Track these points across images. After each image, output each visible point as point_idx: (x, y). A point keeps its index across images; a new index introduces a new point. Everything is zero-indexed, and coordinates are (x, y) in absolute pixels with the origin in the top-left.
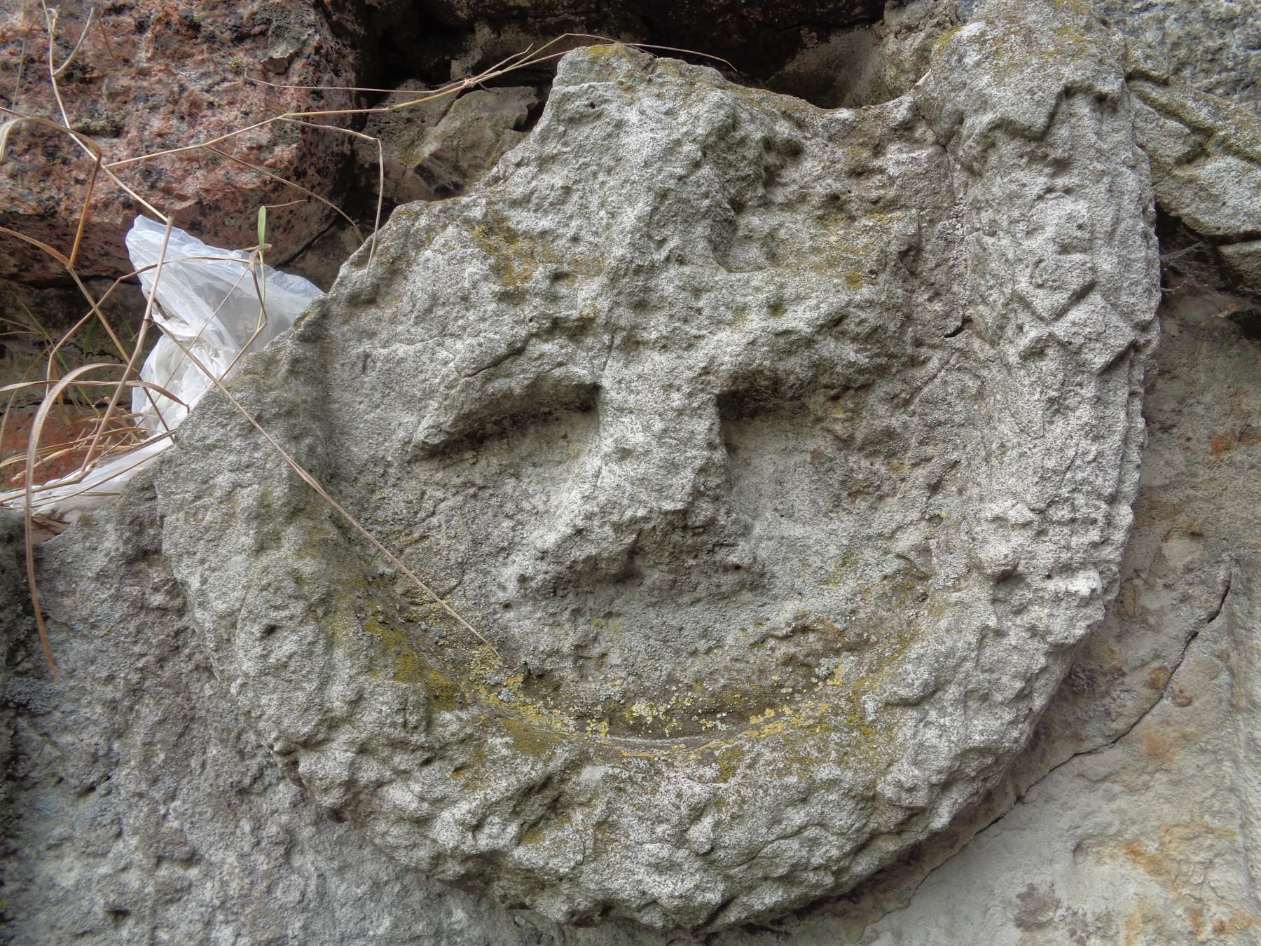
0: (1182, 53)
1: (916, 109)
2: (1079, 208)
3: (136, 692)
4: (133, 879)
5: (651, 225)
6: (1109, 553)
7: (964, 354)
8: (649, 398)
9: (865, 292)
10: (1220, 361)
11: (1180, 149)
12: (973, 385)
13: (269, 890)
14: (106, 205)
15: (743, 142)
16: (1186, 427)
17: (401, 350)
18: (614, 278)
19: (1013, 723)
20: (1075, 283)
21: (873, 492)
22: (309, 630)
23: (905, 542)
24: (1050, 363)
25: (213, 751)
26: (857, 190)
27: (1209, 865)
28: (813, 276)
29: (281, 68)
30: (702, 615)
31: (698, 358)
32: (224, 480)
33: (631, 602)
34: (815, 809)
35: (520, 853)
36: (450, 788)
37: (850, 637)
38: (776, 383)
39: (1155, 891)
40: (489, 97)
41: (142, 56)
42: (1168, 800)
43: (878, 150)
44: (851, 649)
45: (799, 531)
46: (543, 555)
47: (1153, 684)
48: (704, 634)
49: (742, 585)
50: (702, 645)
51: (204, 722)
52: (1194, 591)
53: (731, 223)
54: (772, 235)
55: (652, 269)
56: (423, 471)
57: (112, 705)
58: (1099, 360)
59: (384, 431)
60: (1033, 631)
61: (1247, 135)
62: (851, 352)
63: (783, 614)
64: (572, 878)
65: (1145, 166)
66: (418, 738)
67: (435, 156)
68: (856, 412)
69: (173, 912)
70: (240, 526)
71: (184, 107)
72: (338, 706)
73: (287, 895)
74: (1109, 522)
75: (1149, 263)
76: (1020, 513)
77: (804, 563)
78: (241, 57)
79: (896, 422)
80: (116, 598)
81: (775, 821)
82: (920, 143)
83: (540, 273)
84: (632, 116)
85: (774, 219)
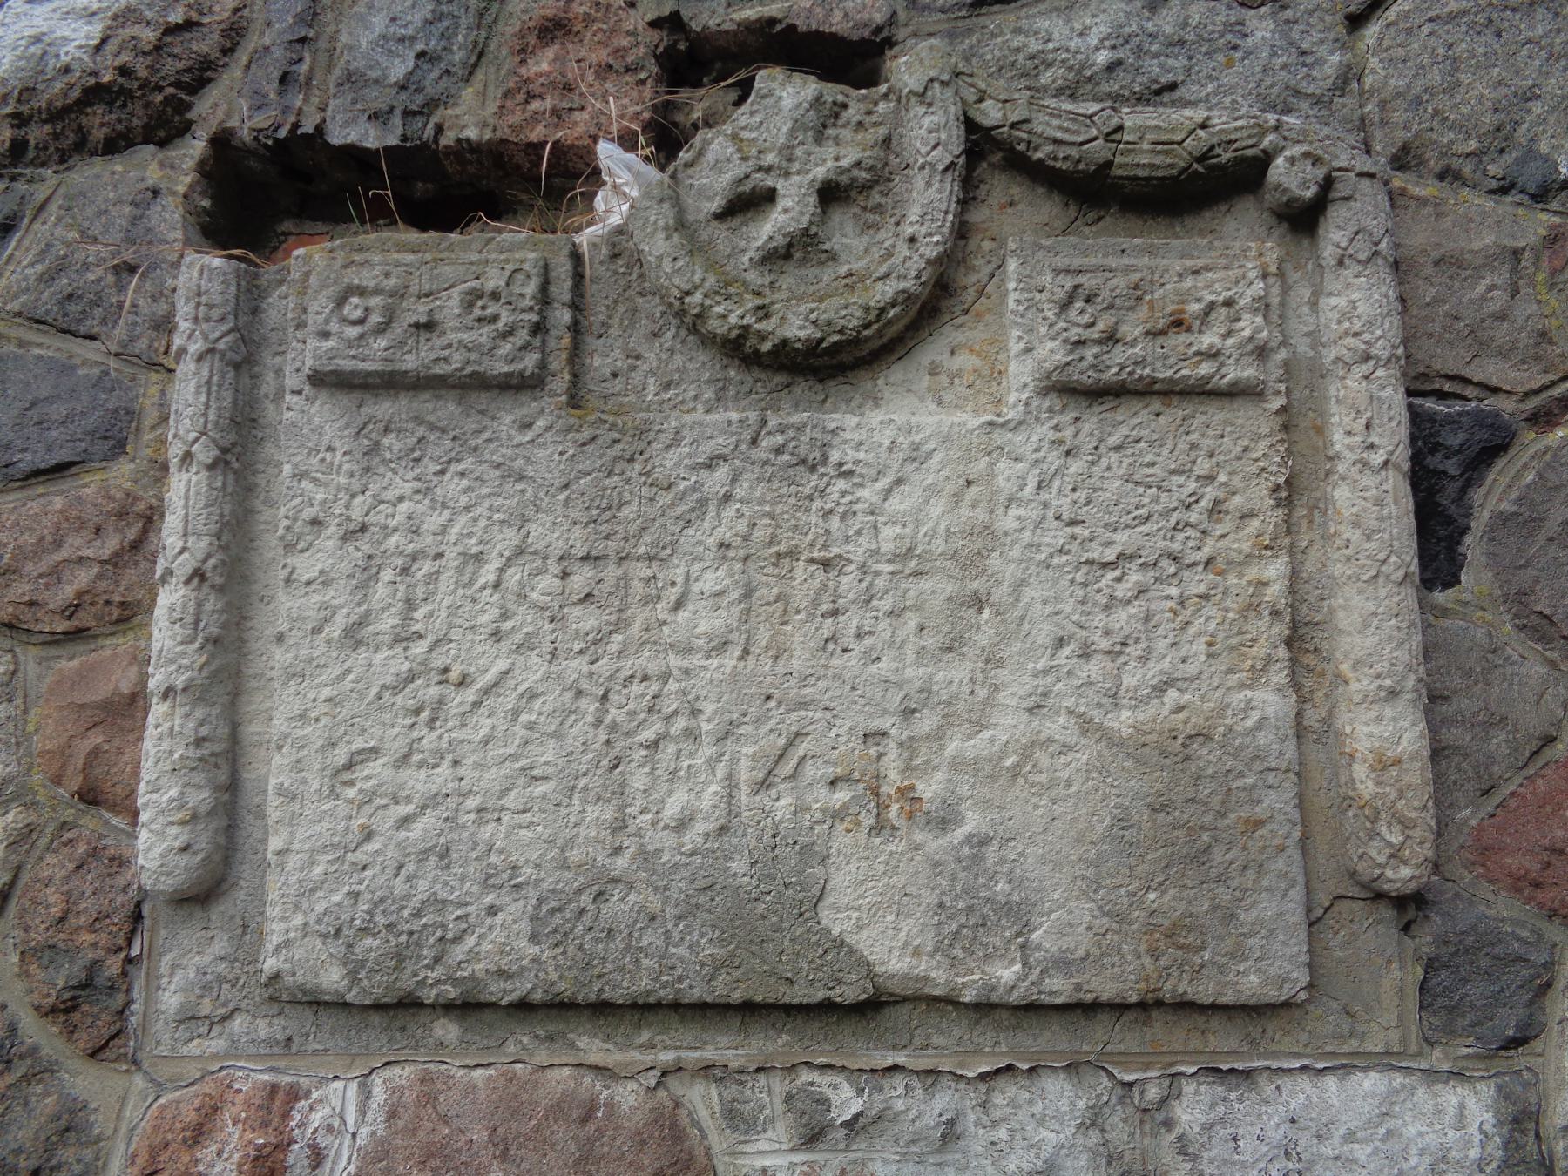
2: (935, 118)
3: (616, 302)
4: (619, 363)
5: (792, 131)
8: (793, 191)
9: (868, 153)
11: (975, 98)
16: (990, 200)
20: (933, 143)
23: (887, 244)
24: (927, 171)
26: (868, 119)
29: (643, 82)
30: (816, 271)
31: (810, 176)
32: (653, 218)
33: (789, 267)
35: (758, 326)
36: (734, 307)
38: (837, 184)
40: (36, 226)
43: (876, 104)
55: (793, 147)
56: (715, 224)
58: (940, 167)
59: (699, 210)
60: (921, 256)
62: (864, 174)
63: (843, 270)
64: (772, 333)
68: (868, 197)
73: (672, 367)
78: (628, 78)
79: (883, 201)
84: (784, 94)
85: (837, 131)
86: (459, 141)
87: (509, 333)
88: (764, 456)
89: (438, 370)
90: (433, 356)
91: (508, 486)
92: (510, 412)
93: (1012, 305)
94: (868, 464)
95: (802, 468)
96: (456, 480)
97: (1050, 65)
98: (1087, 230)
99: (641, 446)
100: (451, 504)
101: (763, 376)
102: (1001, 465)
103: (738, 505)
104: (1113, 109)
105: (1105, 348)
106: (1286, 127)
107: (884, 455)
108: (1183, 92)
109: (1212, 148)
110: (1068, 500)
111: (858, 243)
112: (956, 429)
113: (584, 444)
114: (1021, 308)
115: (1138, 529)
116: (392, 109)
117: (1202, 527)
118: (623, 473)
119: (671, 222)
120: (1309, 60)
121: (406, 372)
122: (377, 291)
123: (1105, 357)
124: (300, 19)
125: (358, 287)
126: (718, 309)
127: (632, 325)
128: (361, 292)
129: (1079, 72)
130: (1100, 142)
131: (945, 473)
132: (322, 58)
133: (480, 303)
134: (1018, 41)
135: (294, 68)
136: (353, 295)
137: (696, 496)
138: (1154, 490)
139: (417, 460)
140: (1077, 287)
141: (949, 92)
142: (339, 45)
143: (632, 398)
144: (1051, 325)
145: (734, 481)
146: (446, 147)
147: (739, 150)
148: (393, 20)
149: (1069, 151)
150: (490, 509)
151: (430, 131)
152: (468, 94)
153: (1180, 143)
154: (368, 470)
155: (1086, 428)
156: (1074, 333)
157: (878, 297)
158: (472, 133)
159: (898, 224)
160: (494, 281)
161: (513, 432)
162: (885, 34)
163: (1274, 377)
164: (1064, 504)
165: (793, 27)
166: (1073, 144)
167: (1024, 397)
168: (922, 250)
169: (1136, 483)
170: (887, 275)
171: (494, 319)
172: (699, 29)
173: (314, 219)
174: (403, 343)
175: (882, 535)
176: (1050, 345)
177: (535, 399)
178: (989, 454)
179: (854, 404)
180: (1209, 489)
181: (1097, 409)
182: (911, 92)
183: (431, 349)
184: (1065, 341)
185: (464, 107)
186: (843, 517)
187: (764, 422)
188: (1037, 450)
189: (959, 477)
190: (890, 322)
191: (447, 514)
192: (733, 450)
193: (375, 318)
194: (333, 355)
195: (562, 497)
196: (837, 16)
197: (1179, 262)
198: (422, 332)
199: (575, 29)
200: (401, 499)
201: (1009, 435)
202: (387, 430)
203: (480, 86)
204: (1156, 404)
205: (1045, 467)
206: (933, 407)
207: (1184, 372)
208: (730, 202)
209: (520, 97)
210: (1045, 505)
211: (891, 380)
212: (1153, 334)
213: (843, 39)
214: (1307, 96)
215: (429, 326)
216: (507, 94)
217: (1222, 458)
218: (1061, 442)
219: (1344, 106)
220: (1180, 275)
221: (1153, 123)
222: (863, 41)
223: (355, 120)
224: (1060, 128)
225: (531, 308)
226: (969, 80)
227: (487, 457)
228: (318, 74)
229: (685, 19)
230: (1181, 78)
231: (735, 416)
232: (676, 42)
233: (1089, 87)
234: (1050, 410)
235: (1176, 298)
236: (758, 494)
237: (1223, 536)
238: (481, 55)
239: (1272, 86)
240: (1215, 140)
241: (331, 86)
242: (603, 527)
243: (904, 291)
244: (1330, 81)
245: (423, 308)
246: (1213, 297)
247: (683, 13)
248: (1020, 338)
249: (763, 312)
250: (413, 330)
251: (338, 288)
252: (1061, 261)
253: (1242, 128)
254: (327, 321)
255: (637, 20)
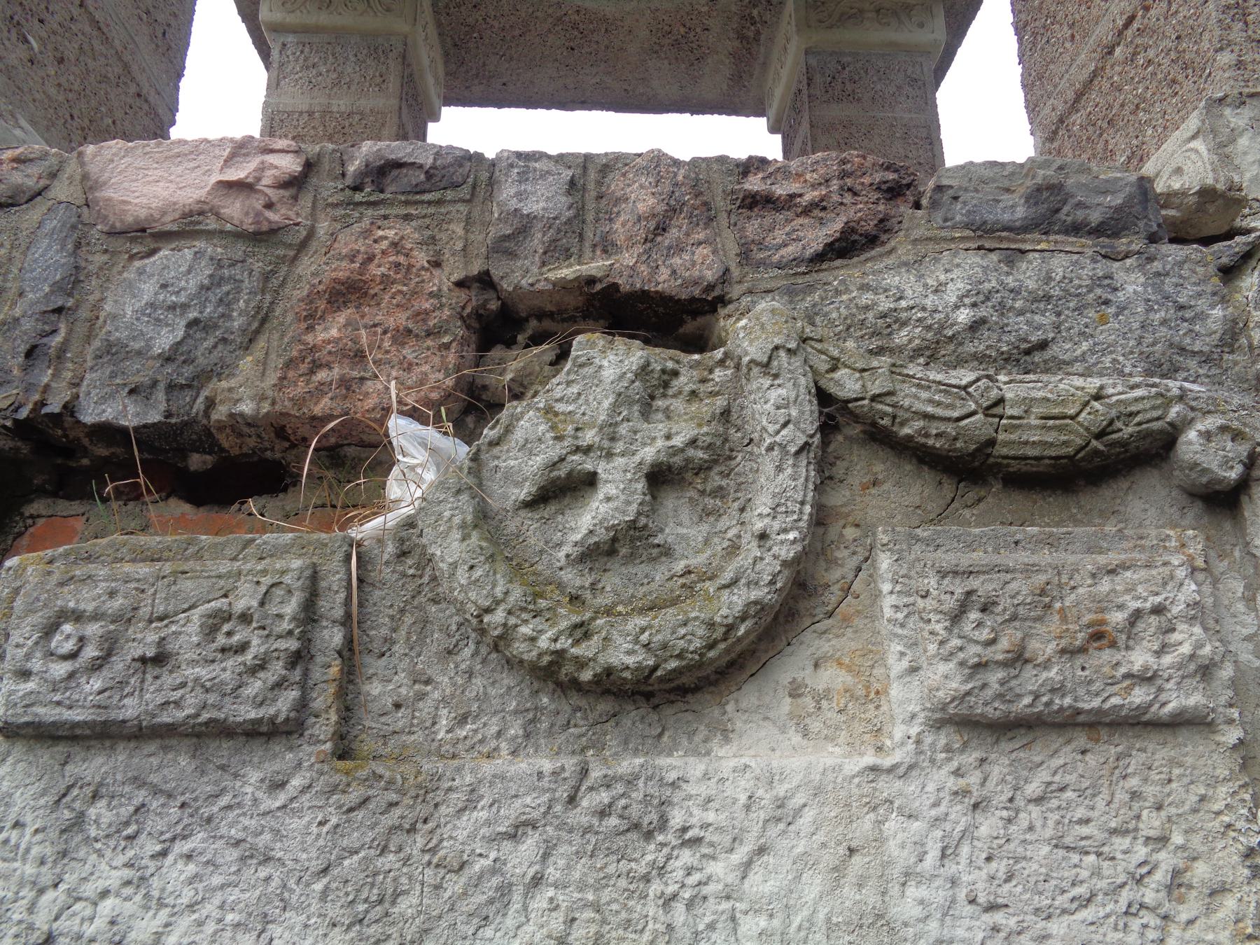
0: (849, 321)
1: (726, 354)
3: (402, 611)
4: (403, 691)
5: (615, 407)
6: (801, 524)
7: (751, 453)
9: (705, 429)
10: (863, 452)
11: (827, 367)
12: (755, 466)
13: (463, 692)
14: (373, 409)
15: (652, 371)
16: (850, 480)
17: (512, 463)
18: (601, 428)
19: (768, 593)
20: (782, 421)
21: (716, 513)
22: (487, 566)
23: (730, 534)
24: (776, 453)
25: (436, 636)
26: (702, 388)
27: (872, 667)
28: (683, 424)
29: (447, 346)
31: (637, 458)
32: (447, 514)
33: (614, 564)
34: (689, 628)
35: (574, 651)
36: (545, 626)
37: (709, 574)
38: (670, 468)
39: (850, 680)
41: (386, 344)
42: (853, 640)
43: (711, 371)
44: (710, 579)
45: (685, 531)
46: (576, 544)
47: (842, 590)
48: (646, 576)
49: (661, 554)
50: (646, 581)
51: (432, 623)
52: (859, 549)
53: (650, 405)
54: (667, 408)
56: (523, 513)
57: (392, 618)
58: (793, 449)
59: (505, 497)
60: (775, 557)
61: (852, 360)
62: (700, 454)
63: (680, 566)
64: (594, 659)
65: (810, 375)
66: (531, 607)
67: (512, 380)
68: (705, 480)
69: (421, 704)
70: (455, 531)
71: (405, 366)
72: (500, 595)
74: (801, 512)
75: (812, 412)
76: (767, 511)
77: (688, 545)
78: (429, 343)
79: (724, 483)
80: (393, 572)
81: (674, 633)
82: (728, 368)
83: (570, 428)
84: (606, 363)
85: (667, 402)
86: (232, 415)
87: (261, 665)
88: (585, 820)
89: (165, 718)
90: (160, 700)
91: (248, 873)
92: (258, 767)
93: (888, 612)
94: (720, 829)
95: (633, 836)
96: (180, 865)
97: (904, 324)
98: (967, 513)
99: (422, 810)
100: (170, 901)
101: (583, 703)
102: (891, 826)
103: (551, 892)
104: (988, 377)
105: (1013, 672)
106: (1191, 395)
107: (740, 815)
108: (1054, 350)
109: (1111, 423)
110: (983, 874)
111: (697, 533)
112: (831, 776)
113: (351, 810)
114: (900, 616)
115: (1081, 915)
116: (155, 383)
117: (1162, 911)
118: (400, 849)
119: (469, 518)
120: (1188, 314)
121: (124, 721)
122: (96, 616)
123: (1013, 683)
124: (58, 288)
125: (73, 611)
126: (525, 630)
127: (422, 640)
128: (77, 617)
129: (939, 332)
130: (979, 416)
131: (820, 837)
132: (81, 329)
133: (226, 628)
134: (866, 299)
135: (45, 340)
136: (67, 620)
137: (495, 881)
138: (1092, 858)
139: (131, 838)
140: (969, 593)
141: (797, 362)
142: (103, 314)
143: (418, 737)
144: (942, 643)
145: (546, 856)
146: (219, 421)
147: (553, 428)
148: (164, 286)
149: (943, 427)
150: (221, 907)
151: (200, 404)
152: (247, 363)
153: (1072, 418)
154: (64, 854)
155: (996, 771)
156: (973, 653)
157: (724, 611)
158: (246, 408)
159: (742, 510)
160: (245, 600)
161: (260, 794)
162: (716, 293)
163: (1223, 700)
164: (976, 879)
165: (615, 286)
166: (949, 419)
167: (914, 730)
168: (775, 549)
169: (1068, 848)
170: (734, 583)
171: (243, 647)
172: (511, 289)
173: (70, 498)
174: (122, 684)
175: (742, 930)
176: (943, 668)
177: (291, 749)
178: (874, 809)
179: (698, 738)
180: (1162, 855)
181: (1006, 746)
182: (752, 361)
183: (159, 690)
184: (962, 664)
185: (240, 379)
186: (690, 905)
187: (584, 772)
188: (936, 804)
189: (839, 843)
190: (739, 640)
191: (164, 914)
192: (545, 814)
193: (90, 652)
194: (31, 701)
195: (318, 887)
196: (664, 274)
197: (1088, 558)
198: (149, 668)
199: (372, 292)
200: (105, 894)
201: (898, 784)
202: (95, 796)
203: (259, 354)
204: (1081, 740)
205: (948, 827)
206: (797, 739)
207: (1115, 701)
208: (541, 488)
209: (304, 367)
210: (954, 882)
211: (743, 705)
212: (1069, 652)
213: (671, 298)
214: (1194, 353)
215: (160, 659)
216: (290, 363)
217: (1173, 810)
218: (966, 792)
219: (1236, 363)
220: (1093, 576)
221: (1040, 394)
222: (693, 300)
223: (112, 396)
224: (931, 401)
225: (290, 633)
226: (818, 346)
227: (223, 830)
228: (75, 346)
229: (496, 279)
230: (1051, 335)
231: (547, 766)
232: (486, 301)
233: (952, 347)
234: (948, 749)
235: (1093, 606)
236: (577, 875)
237: (1190, 922)
238: (264, 321)
239: (1154, 344)
240: (1114, 413)
241: (89, 358)
242: (371, 930)
243: (756, 603)
244: (1218, 336)
245: (152, 637)
246: (1138, 604)
247: (492, 271)
248: (902, 654)
249: (582, 631)
250: (138, 664)
251: (47, 612)
252: (947, 558)
253: (1143, 398)
254: (28, 657)
255: (442, 280)
